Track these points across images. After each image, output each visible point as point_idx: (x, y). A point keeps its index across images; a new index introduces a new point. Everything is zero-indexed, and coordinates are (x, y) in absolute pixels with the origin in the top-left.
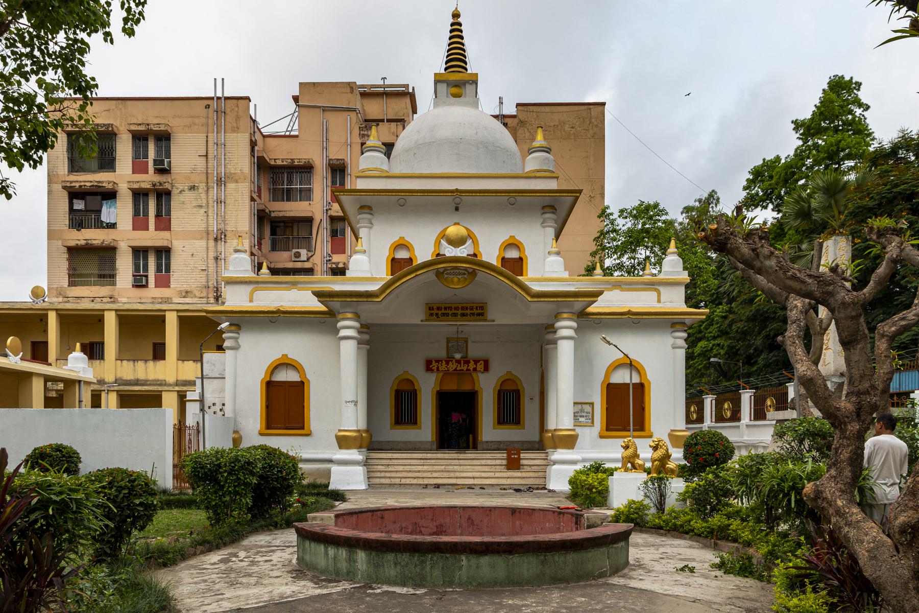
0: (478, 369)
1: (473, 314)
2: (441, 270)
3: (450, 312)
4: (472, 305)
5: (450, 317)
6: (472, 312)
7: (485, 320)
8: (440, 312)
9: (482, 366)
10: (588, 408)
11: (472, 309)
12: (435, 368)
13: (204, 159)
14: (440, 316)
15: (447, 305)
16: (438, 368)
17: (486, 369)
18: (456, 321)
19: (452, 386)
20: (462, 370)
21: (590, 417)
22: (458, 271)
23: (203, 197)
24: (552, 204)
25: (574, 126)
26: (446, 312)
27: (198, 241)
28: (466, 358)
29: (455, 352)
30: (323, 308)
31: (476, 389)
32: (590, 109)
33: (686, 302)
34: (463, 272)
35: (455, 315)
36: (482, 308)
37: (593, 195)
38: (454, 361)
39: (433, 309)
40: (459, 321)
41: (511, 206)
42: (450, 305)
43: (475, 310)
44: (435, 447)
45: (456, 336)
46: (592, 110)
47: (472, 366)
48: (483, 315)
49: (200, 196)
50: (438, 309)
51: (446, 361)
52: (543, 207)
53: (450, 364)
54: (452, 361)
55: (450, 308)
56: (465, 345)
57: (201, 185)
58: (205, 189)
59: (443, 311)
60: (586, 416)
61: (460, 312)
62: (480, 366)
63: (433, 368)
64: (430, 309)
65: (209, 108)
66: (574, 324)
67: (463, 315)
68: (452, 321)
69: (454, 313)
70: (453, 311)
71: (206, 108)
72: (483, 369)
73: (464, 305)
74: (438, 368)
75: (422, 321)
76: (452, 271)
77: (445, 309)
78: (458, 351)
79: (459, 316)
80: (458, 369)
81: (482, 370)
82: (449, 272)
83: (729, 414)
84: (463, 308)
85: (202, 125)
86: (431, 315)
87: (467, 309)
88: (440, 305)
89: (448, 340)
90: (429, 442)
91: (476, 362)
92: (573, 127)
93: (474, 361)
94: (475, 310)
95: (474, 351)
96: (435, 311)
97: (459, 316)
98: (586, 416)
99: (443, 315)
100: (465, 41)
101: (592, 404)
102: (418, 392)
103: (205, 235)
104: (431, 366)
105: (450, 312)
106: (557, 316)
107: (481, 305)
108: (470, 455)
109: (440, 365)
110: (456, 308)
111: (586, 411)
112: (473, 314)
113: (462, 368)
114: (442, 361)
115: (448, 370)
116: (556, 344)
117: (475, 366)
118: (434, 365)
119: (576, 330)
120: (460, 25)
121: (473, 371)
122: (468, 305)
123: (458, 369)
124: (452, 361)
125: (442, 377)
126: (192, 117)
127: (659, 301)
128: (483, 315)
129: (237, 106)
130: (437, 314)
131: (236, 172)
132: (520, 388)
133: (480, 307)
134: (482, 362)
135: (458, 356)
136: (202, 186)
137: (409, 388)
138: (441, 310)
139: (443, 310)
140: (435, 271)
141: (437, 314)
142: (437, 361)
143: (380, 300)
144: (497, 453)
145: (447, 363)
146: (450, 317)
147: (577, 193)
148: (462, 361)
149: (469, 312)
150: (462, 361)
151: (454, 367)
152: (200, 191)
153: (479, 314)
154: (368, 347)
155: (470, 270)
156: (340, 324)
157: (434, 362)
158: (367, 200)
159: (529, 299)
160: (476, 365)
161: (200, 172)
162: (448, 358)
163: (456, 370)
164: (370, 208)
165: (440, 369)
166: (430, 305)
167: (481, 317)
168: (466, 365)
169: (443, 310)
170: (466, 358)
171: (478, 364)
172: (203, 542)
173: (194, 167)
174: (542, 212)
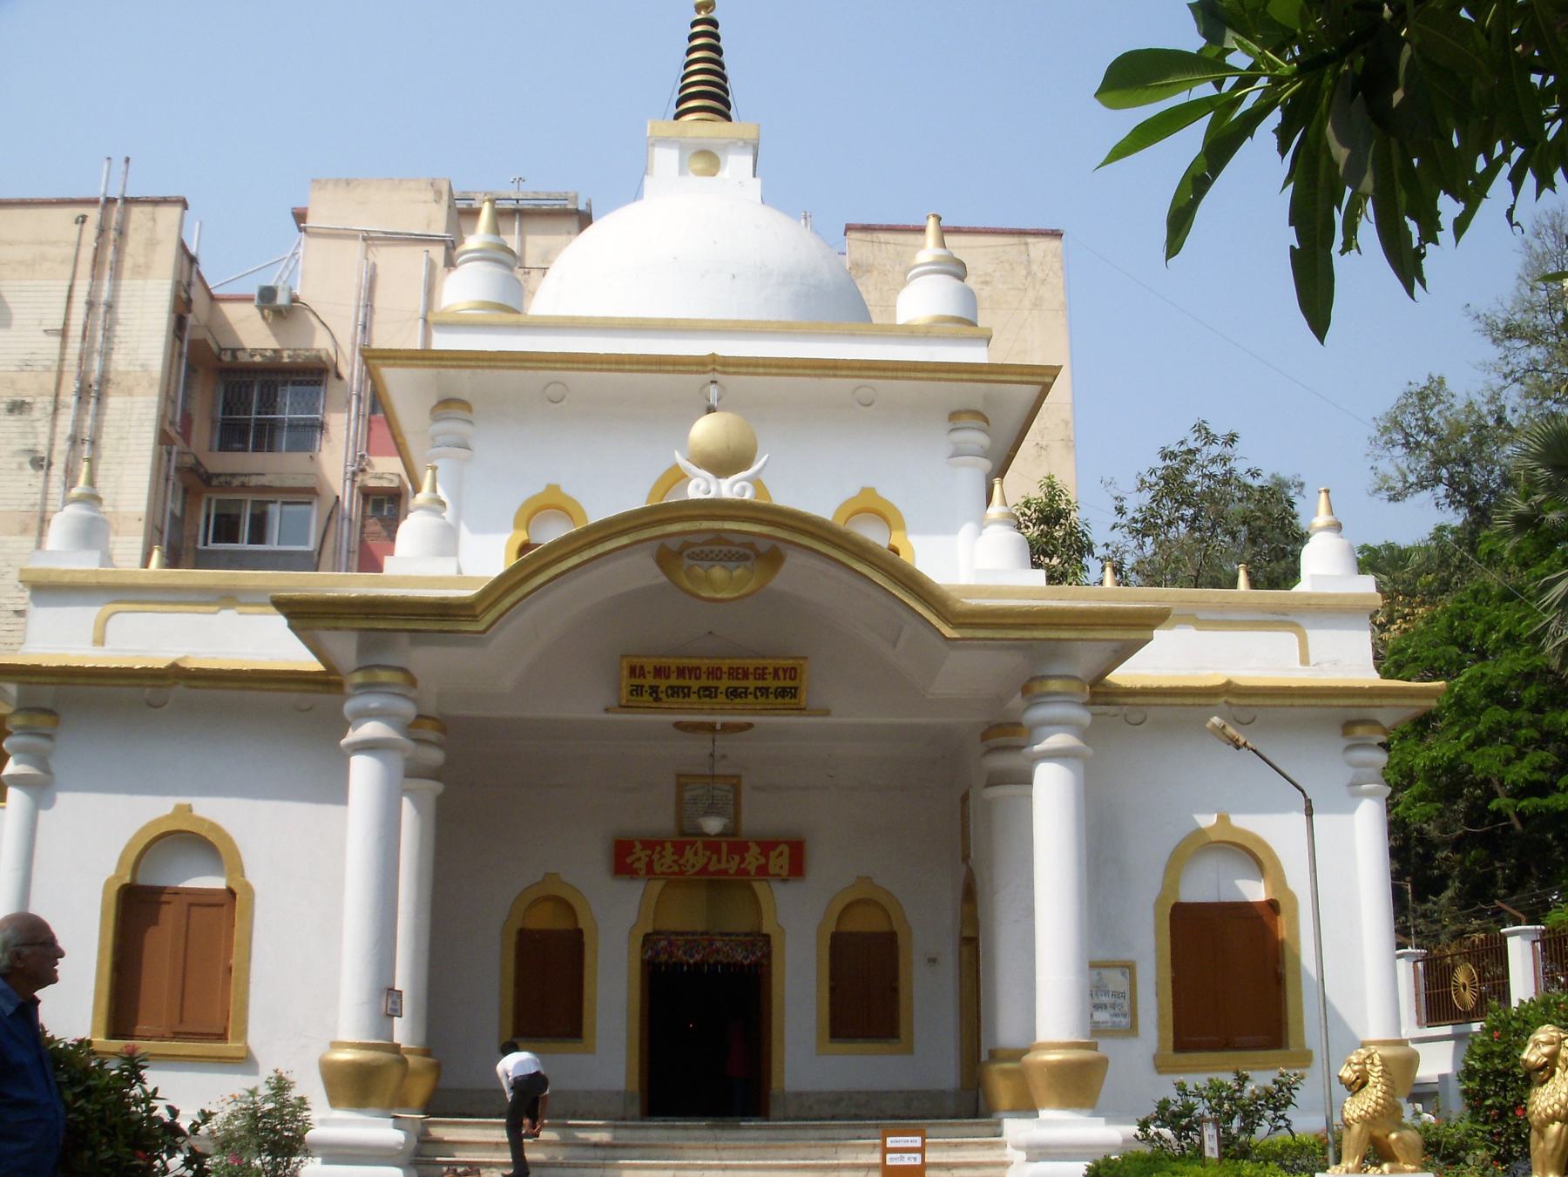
0: (772, 869)
1: (765, 691)
2: (674, 544)
3: (695, 685)
4: (762, 663)
5: (694, 697)
6: (761, 684)
7: (800, 710)
8: (663, 684)
9: (785, 861)
10: (1116, 980)
11: (761, 673)
12: (641, 865)
13: (57, 340)
14: (663, 696)
15: (686, 662)
16: (650, 865)
17: (797, 868)
18: (713, 711)
19: (688, 916)
20: (725, 872)
21: (1126, 1008)
22: (725, 549)
23: (40, 429)
24: (979, 407)
25: (988, 279)
26: (681, 682)
27: (14, 538)
28: (733, 835)
29: (706, 814)
30: (306, 661)
31: (765, 931)
32: (1026, 244)
33: (1378, 668)
34: (742, 550)
35: (709, 692)
36: (792, 672)
37: (1043, 443)
38: (700, 845)
39: (643, 674)
40: (722, 711)
41: (864, 409)
42: (695, 662)
43: (770, 677)
44: (636, 1109)
45: (707, 771)
46: (1031, 247)
47: (753, 859)
48: (794, 696)
49: (33, 427)
50: (659, 672)
51: (674, 844)
52: (954, 416)
53: (689, 853)
54: (693, 844)
55: (694, 672)
56: (731, 796)
57: (39, 399)
58: (50, 409)
59: (673, 681)
60: (1113, 1006)
61: (724, 684)
62: (779, 861)
63: (636, 865)
64: (633, 671)
65: (83, 222)
66: (1083, 715)
67: (733, 693)
68: (701, 711)
69: (706, 689)
70: (704, 682)
71: (77, 222)
72: (786, 867)
73: (737, 663)
74: (650, 865)
75: (607, 710)
76: (707, 549)
77: (681, 672)
78: (712, 810)
79: (722, 698)
80: (712, 868)
81: (785, 872)
82: (697, 549)
83: (1469, 997)
84: (734, 673)
85: (63, 262)
86: (637, 690)
87: (746, 675)
88: (664, 662)
89: (682, 782)
90: (618, 1093)
91: (767, 846)
92: (986, 283)
93: (759, 844)
94: (770, 677)
95: (761, 817)
96: (650, 680)
97: (722, 698)
98: (1113, 1006)
99: (675, 691)
100: (725, 59)
101: (1129, 968)
102: (586, 938)
103: (35, 525)
104: (629, 860)
105: (695, 685)
106: (1031, 689)
107: (790, 663)
108: (751, 1131)
109: (656, 857)
110: (714, 673)
111: (1111, 987)
112: (765, 691)
113: (723, 866)
114: (662, 844)
115: (682, 873)
116: (1030, 782)
117: (762, 861)
118: (640, 855)
119: (1085, 734)
120: (714, 24)
121: (757, 874)
122: (751, 664)
123: (712, 868)
124: (693, 844)
125: (661, 894)
126: (41, 243)
127: (1305, 660)
128: (794, 696)
129: (154, 220)
130: (654, 690)
131: (131, 368)
132: (895, 928)
133: (785, 671)
134: (785, 849)
135: (713, 825)
136: (43, 403)
137: (561, 924)
138: (668, 677)
139: (674, 676)
140: (657, 543)
141: (654, 690)
142: (649, 844)
143: (481, 627)
144: (840, 1127)
145: (679, 848)
146: (694, 697)
147: (1047, 375)
148: (724, 847)
149: (751, 684)
150: (724, 847)
151: (700, 862)
152: (36, 414)
153: (783, 692)
154: (438, 787)
155: (763, 546)
156: (350, 706)
157: (638, 847)
158: (463, 381)
159: (948, 632)
160: (767, 857)
161: (40, 369)
162: (682, 833)
163: (704, 870)
164: (464, 405)
165: (657, 868)
166: (637, 662)
167: (787, 700)
168: (737, 858)
169: (674, 676)
170: (733, 835)
171: (773, 854)
172: (1210, 583)
173: (27, 357)
174: (951, 426)
